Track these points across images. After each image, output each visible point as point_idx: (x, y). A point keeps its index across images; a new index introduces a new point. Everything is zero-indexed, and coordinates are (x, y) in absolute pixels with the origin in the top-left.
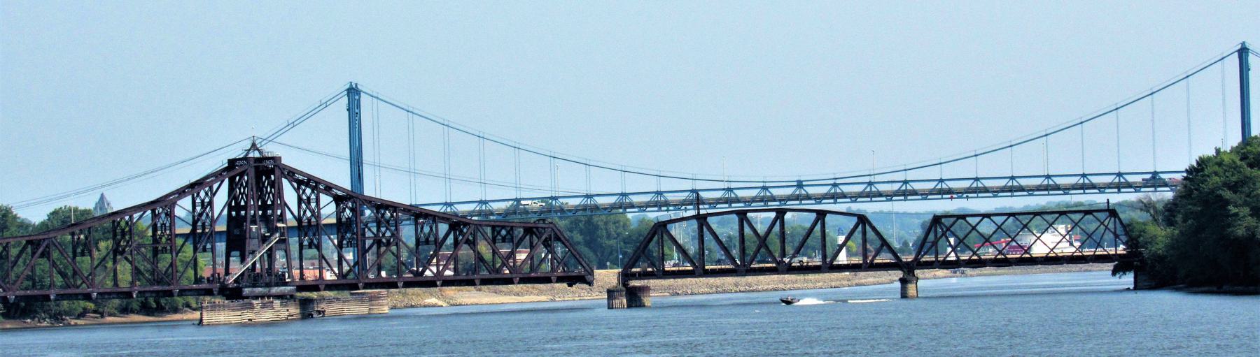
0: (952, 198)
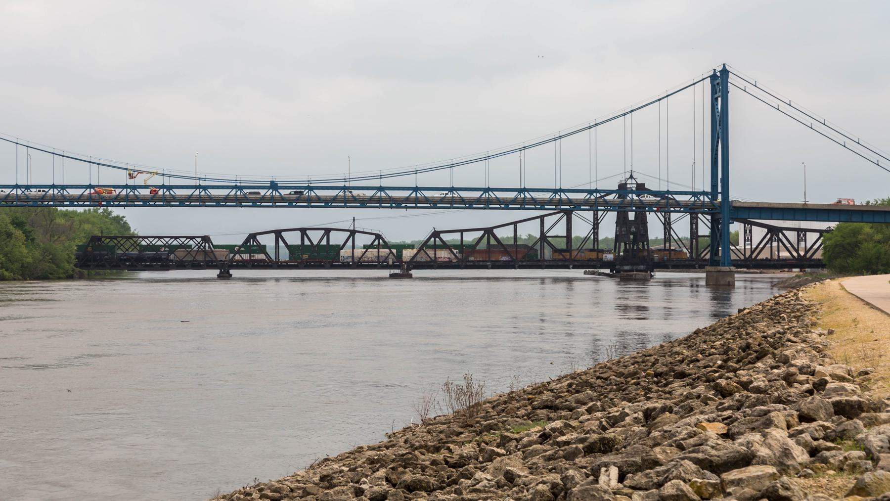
0: (391, 207)
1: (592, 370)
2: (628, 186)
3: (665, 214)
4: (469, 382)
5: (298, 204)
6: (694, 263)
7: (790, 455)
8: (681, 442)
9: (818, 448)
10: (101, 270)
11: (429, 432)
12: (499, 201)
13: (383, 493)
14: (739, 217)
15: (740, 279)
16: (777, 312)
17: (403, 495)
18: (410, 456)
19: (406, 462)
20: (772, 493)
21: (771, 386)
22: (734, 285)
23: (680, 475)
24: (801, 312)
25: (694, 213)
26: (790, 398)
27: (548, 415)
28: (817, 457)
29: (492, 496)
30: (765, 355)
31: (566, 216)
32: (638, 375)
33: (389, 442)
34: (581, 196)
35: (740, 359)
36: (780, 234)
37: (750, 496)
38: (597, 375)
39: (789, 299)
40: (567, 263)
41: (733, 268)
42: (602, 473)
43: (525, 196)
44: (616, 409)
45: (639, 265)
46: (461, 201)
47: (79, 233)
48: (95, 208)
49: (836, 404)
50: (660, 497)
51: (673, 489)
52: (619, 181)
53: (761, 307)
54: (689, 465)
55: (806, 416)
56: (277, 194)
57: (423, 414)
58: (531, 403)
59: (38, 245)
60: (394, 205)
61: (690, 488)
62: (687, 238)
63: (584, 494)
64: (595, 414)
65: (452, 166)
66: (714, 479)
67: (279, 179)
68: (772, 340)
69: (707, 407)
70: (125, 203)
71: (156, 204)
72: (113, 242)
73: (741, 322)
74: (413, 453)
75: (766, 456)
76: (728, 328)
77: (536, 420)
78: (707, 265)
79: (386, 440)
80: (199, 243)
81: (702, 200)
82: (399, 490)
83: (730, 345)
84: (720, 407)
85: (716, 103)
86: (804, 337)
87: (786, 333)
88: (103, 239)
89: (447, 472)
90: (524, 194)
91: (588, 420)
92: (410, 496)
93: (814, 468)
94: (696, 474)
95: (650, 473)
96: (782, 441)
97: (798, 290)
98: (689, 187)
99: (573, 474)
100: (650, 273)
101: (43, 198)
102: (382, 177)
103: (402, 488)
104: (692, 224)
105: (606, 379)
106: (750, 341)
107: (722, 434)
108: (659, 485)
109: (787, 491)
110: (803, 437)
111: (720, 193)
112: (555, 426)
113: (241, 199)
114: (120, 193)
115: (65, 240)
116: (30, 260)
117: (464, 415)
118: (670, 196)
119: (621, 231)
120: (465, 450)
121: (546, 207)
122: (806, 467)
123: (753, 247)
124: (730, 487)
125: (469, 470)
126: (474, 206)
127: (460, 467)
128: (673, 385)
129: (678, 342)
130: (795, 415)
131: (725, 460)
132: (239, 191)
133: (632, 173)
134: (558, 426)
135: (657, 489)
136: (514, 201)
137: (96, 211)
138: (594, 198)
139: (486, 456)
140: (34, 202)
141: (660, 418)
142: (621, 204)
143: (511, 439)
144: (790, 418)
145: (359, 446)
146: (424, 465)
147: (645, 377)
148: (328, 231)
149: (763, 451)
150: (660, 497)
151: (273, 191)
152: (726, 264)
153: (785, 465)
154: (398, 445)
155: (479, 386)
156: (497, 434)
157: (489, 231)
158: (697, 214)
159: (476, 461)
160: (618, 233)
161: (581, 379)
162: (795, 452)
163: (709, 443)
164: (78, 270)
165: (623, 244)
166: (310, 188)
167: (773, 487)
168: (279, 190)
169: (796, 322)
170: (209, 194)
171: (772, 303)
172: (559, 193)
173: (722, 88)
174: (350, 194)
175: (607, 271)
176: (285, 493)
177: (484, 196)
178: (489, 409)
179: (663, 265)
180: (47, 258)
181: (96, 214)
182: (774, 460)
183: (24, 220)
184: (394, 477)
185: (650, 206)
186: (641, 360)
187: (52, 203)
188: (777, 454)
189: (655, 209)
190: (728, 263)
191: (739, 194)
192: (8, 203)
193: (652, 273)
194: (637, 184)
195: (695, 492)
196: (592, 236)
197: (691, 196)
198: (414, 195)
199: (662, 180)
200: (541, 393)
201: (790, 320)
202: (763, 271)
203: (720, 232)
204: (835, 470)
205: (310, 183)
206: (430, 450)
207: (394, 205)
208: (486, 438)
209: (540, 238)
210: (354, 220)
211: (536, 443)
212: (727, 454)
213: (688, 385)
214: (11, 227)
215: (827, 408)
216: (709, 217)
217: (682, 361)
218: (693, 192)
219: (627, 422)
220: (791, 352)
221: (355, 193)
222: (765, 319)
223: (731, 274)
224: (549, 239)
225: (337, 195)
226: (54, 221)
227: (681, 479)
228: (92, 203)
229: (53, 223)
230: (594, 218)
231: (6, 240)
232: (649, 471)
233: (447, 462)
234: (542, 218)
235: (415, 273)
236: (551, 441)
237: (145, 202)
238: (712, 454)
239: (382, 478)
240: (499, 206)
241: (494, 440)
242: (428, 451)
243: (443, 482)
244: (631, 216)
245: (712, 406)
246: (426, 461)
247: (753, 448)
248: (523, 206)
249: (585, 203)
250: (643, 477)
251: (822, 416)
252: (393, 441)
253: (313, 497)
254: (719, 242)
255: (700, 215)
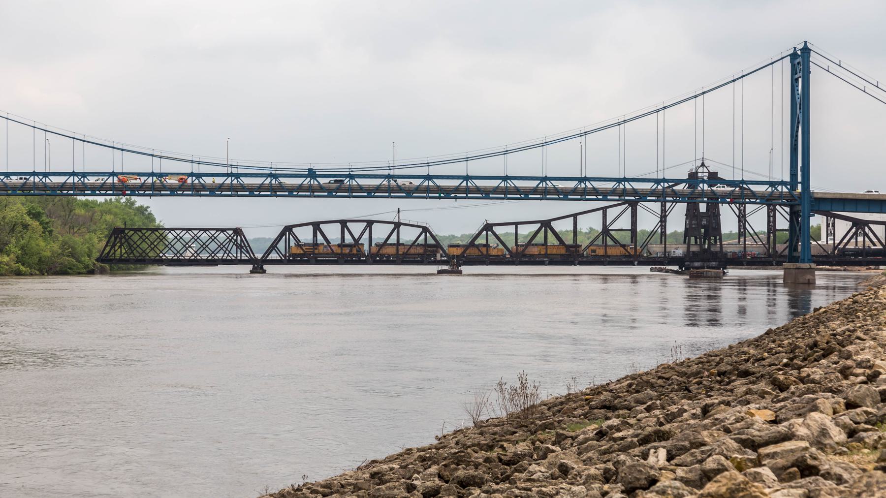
0: (440, 198)
1: (654, 371)
2: (700, 175)
3: (739, 206)
4: (524, 382)
5: (338, 194)
6: (771, 259)
7: (827, 435)
8: (728, 426)
9: (856, 429)
10: (124, 265)
11: (481, 434)
12: (557, 191)
13: (436, 488)
14: (820, 209)
15: (821, 278)
16: (853, 311)
17: (456, 490)
18: (463, 454)
19: (459, 460)
20: (801, 462)
21: (826, 378)
22: (815, 283)
23: (722, 452)
24: (878, 311)
25: (771, 204)
26: (841, 388)
27: (606, 415)
28: (855, 438)
29: (545, 485)
30: (831, 353)
31: (630, 208)
32: (702, 375)
33: (439, 444)
34: (648, 186)
35: (806, 356)
36: (866, 227)
37: (781, 466)
38: (659, 375)
39: (867, 298)
40: (631, 259)
41: (813, 265)
42: (650, 454)
43: (586, 186)
44: (674, 407)
45: (711, 261)
46: (516, 190)
47: (100, 225)
48: (117, 197)
49: (883, 393)
50: (702, 470)
51: (714, 464)
52: (689, 170)
53: (838, 306)
54: (731, 443)
55: (853, 404)
56: (316, 183)
57: (475, 417)
58: (589, 404)
59: (56, 237)
60: (442, 195)
61: (731, 463)
62: (765, 232)
63: (631, 469)
64: (654, 411)
65: (506, 152)
66: (753, 456)
67: (319, 165)
68: (841, 338)
69: (764, 400)
70: (151, 192)
71: (337, 194)
72: (155, 234)
73: (815, 322)
74: (465, 451)
75: (805, 435)
76: (801, 328)
77: (594, 419)
78: (785, 262)
79: (435, 442)
80: (230, 236)
81: (780, 190)
82: (452, 485)
83: (797, 343)
84: (775, 400)
85: (796, 84)
86: (874, 334)
87: (856, 330)
88: (126, 232)
89: (501, 469)
90: (585, 184)
91: (646, 417)
92: (463, 491)
93: (850, 447)
94: (738, 452)
95: (695, 452)
96: (820, 422)
97: (879, 288)
98: (766, 176)
99: (624, 459)
100: (723, 270)
101: (63, 186)
102: (429, 164)
103: (455, 483)
104: (769, 217)
105: (668, 379)
106: (818, 338)
107: (770, 421)
108: (701, 462)
109: (815, 460)
110: (842, 419)
111: (800, 183)
112: (612, 423)
113: (276, 188)
114: (145, 181)
115: (85, 232)
116: (48, 254)
117: (519, 418)
118: (745, 186)
119: (691, 224)
120: (519, 448)
121: (609, 197)
122: (843, 446)
123: (836, 242)
124: (766, 460)
125: (523, 466)
126: (569, 197)
127: (514, 465)
128: (736, 383)
129: (747, 343)
130: (842, 403)
131: (766, 440)
132: (274, 180)
133: (703, 161)
134: (615, 424)
135: (700, 464)
136: (574, 191)
137: (118, 201)
138: (661, 188)
139: (541, 453)
140: (14, 190)
141: (715, 410)
142: (691, 194)
143: (567, 437)
144: (837, 406)
145: (408, 448)
146: (477, 462)
147: (708, 377)
148: (370, 223)
149: (802, 431)
150: (702, 470)
151: (311, 180)
152: (806, 260)
153: (822, 444)
154: (449, 446)
155: (534, 387)
156: (553, 433)
157: (546, 224)
158: (775, 206)
159: (530, 459)
160: (688, 227)
161: (642, 380)
162: (833, 432)
163: (754, 427)
164: (99, 264)
165: (693, 239)
166: (352, 177)
167: (802, 457)
168: (355, 179)
169: (870, 320)
170: (241, 182)
171: (849, 302)
172: (623, 183)
173: (803, 67)
174: (395, 184)
175: (676, 268)
176: (335, 488)
177: (541, 185)
178: (544, 411)
179: (740, 260)
180: (67, 251)
181: (118, 204)
182: (812, 439)
183: (40, 210)
184: (446, 473)
185: (724, 198)
186: (706, 360)
187: (72, 192)
188: (815, 434)
189: (728, 200)
190: (809, 260)
191: (820, 185)
192: (25, 192)
193: (725, 271)
194: (710, 173)
195: (736, 467)
196: (659, 229)
197: (768, 186)
198: (464, 184)
199: (737, 168)
200: (599, 393)
201: (865, 318)
202: (847, 268)
203: (799, 225)
204: (869, 449)
205: (352, 171)
206: (483, 448)
207: (442, 195)
208: (542, 437)
209: (601, 232)
210: (399, 212)
211: (592, 439)
212: (768, 434)
213: (750, 383)
214: (28, 218)
215: (873, 396)
216: (788, 209)
217: (747, 361)
218: (770, 181)
219: (685, 417)
220: (854, 347)
221: (400, 181)
222: (840, 318)
223: (811, 271)
224: (612, 233)
225: (381, 184)
226: (74, 211)
227: (722, 455)
228: (233, 193)
229: (72, 213)
230: (662, 210)
231: (21, 231)
232: (695, 450)
233: (500, 460)
234: (604, 210)
235: (465, 269)
236: (607, 438)
237: (173, 191)
238: (754, 434)
239: (435, 475)
240: (595, 197)
241: (549, 439)
242: (481, 449)
243: (497, 478)
244: (703, 208)
245: (769, 399)
246: (480, 458)
247: (793, 430)
248: (584, 197)
249: (652, 194)
250: (689, 456)
251: (869, 404)
252: (444, 443)
253: (365, 492)
254: (798, 236)
255: (778, 207)
